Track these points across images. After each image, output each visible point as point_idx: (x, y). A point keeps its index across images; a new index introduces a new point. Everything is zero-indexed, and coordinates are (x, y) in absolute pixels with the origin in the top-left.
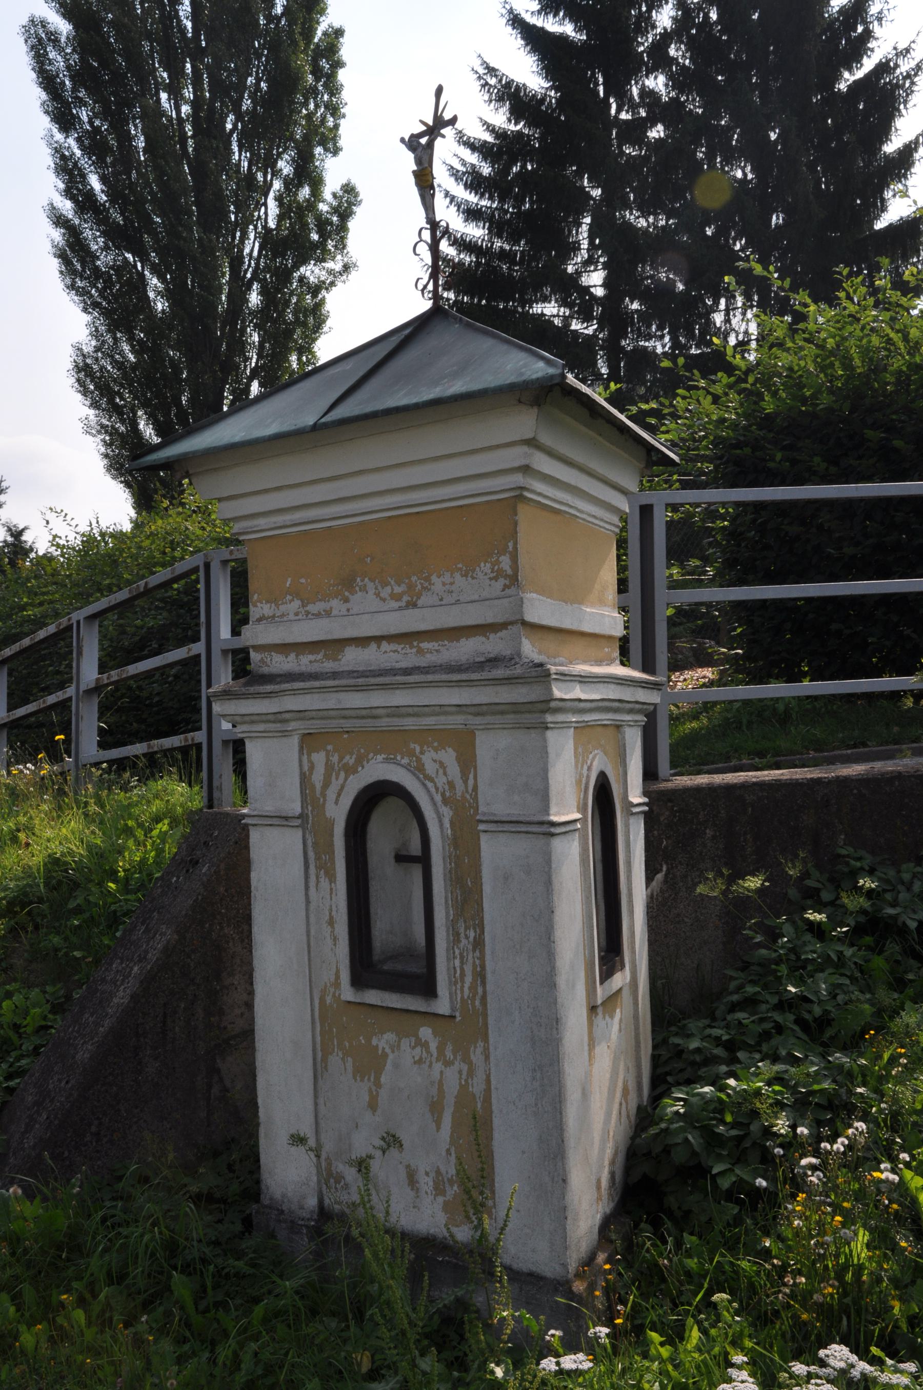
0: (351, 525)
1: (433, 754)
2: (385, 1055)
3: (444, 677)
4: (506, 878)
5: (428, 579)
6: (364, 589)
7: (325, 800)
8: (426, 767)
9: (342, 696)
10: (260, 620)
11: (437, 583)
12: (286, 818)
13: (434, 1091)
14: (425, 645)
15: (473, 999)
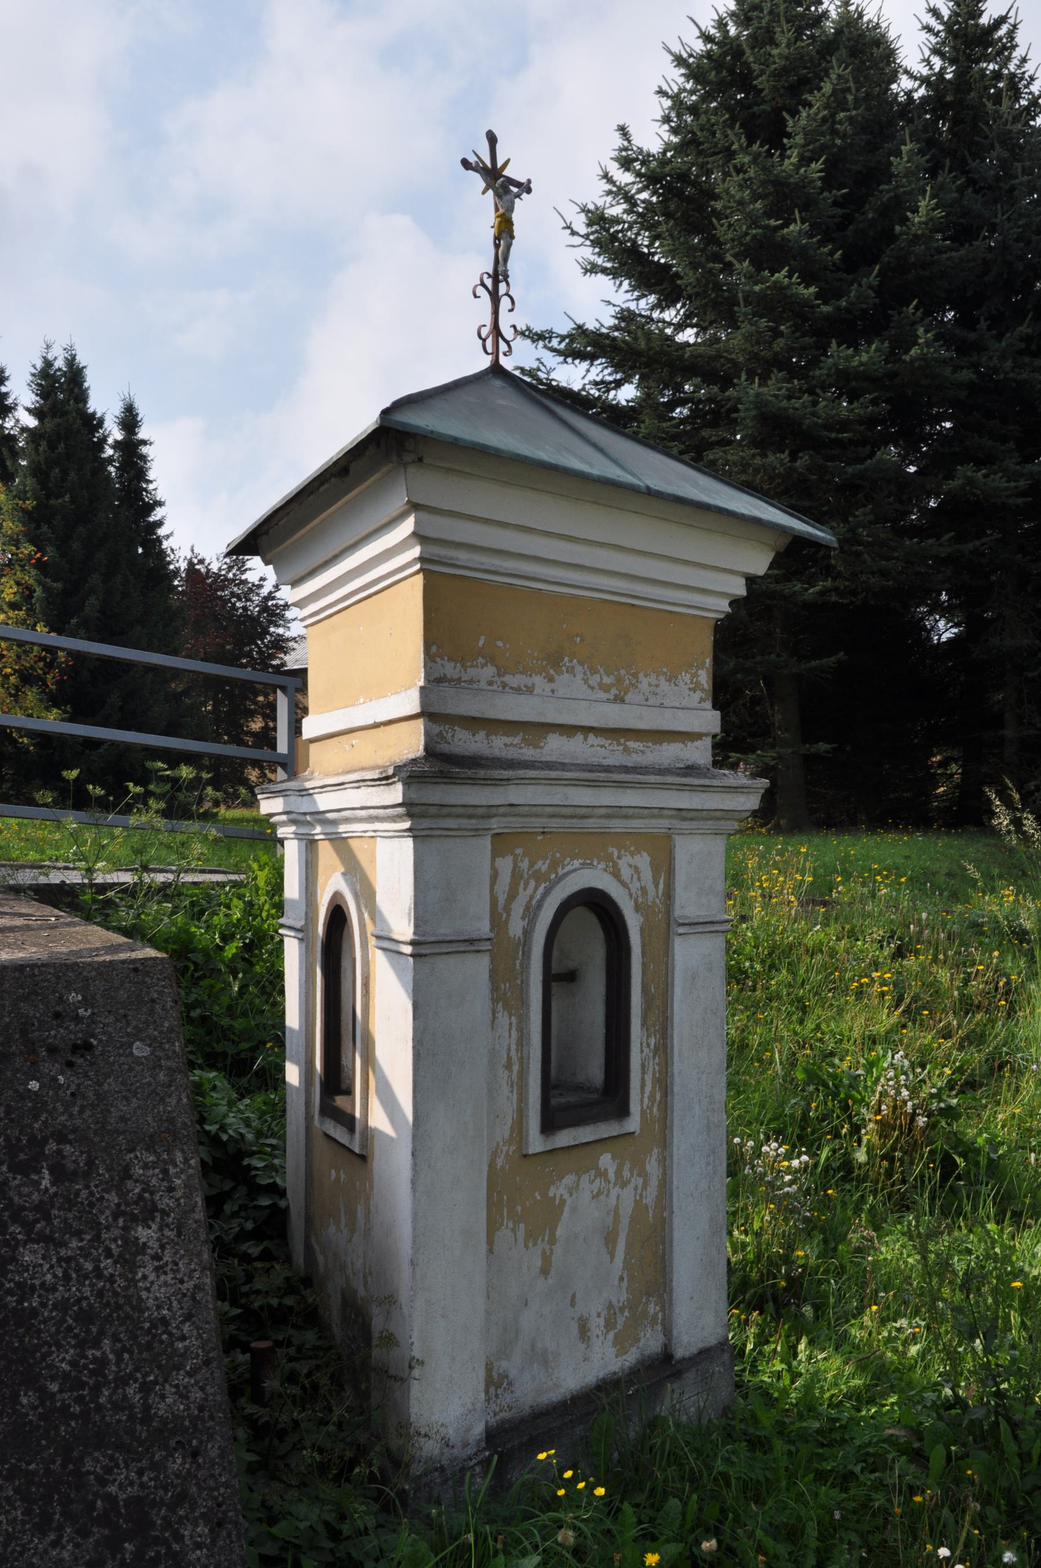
0: (563, 596)
2: (563, 1202)
5: (635, 676)
6: (571, 671)
7: (509, 915)
8: (623, 872)
9: (571, 791)
12: (471, 941)
13: (610, 1220)
14: (631, 744)
15: (650, 1108)
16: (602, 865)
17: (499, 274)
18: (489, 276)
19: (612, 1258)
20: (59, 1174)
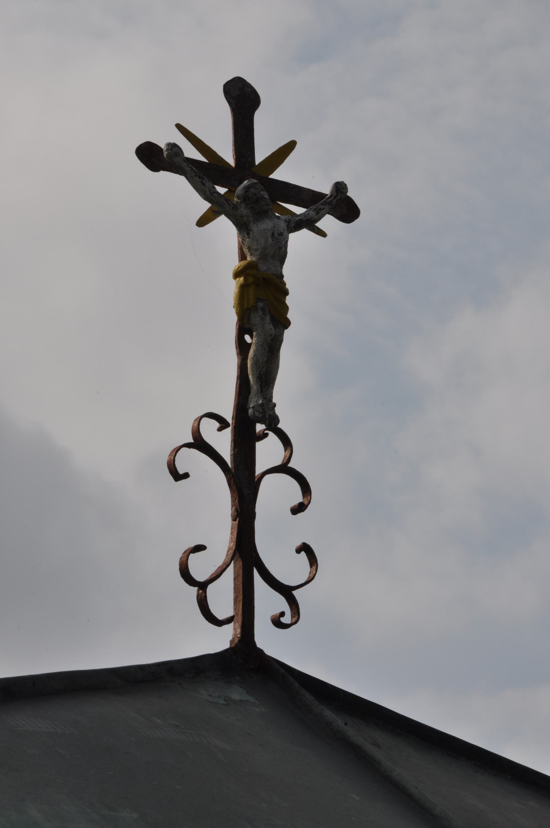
17: (253, 415)
18: (223, 424)
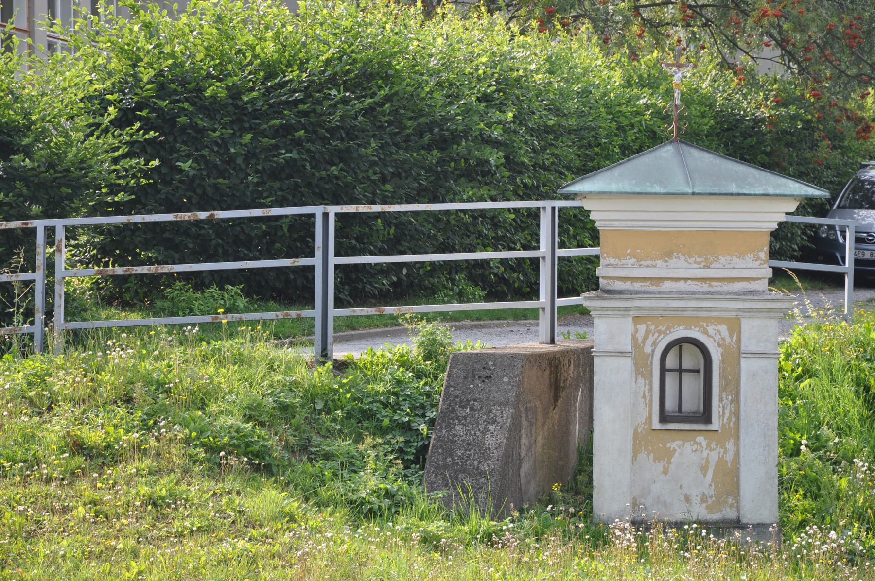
1: (714, 327)
3: (733, 297)
4: (754, 375)
5: (717, 257)
10: (607, 265)
11: (722, 260)
12: (622, 353)
13: (704, 462)
14: (714, 283)
16: (697, 329)
19: (705, 476)
20: (472, 409)
